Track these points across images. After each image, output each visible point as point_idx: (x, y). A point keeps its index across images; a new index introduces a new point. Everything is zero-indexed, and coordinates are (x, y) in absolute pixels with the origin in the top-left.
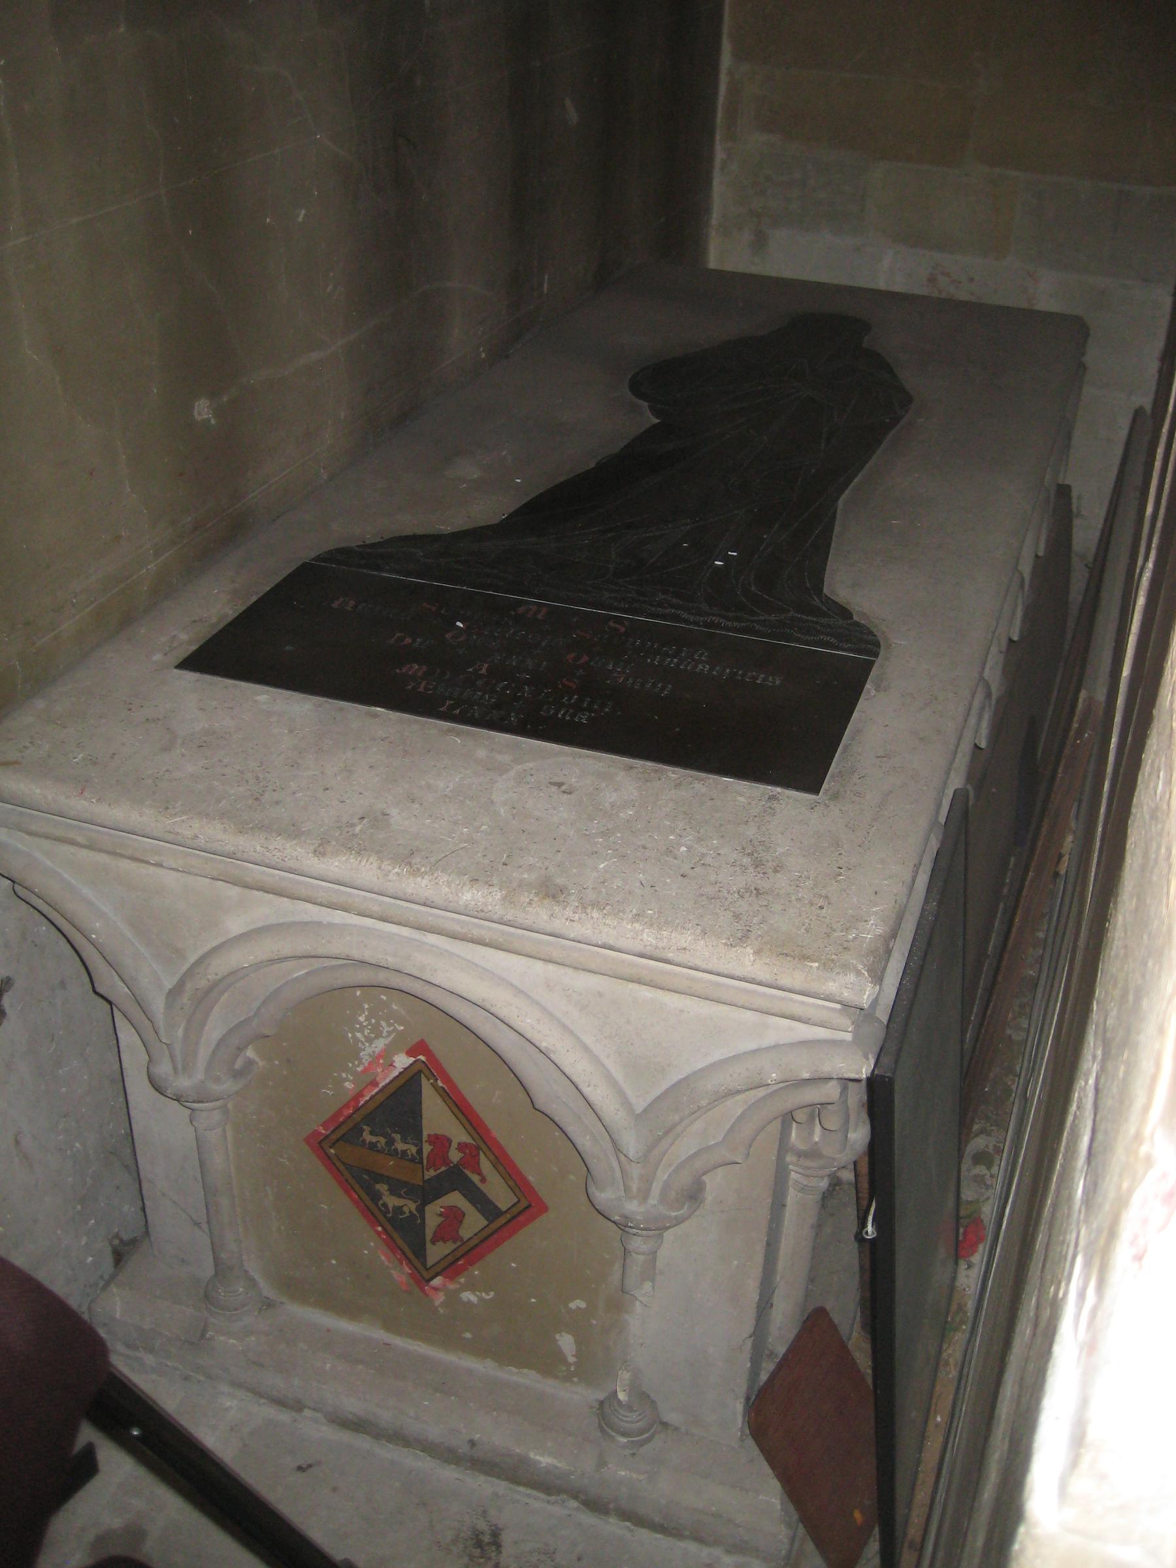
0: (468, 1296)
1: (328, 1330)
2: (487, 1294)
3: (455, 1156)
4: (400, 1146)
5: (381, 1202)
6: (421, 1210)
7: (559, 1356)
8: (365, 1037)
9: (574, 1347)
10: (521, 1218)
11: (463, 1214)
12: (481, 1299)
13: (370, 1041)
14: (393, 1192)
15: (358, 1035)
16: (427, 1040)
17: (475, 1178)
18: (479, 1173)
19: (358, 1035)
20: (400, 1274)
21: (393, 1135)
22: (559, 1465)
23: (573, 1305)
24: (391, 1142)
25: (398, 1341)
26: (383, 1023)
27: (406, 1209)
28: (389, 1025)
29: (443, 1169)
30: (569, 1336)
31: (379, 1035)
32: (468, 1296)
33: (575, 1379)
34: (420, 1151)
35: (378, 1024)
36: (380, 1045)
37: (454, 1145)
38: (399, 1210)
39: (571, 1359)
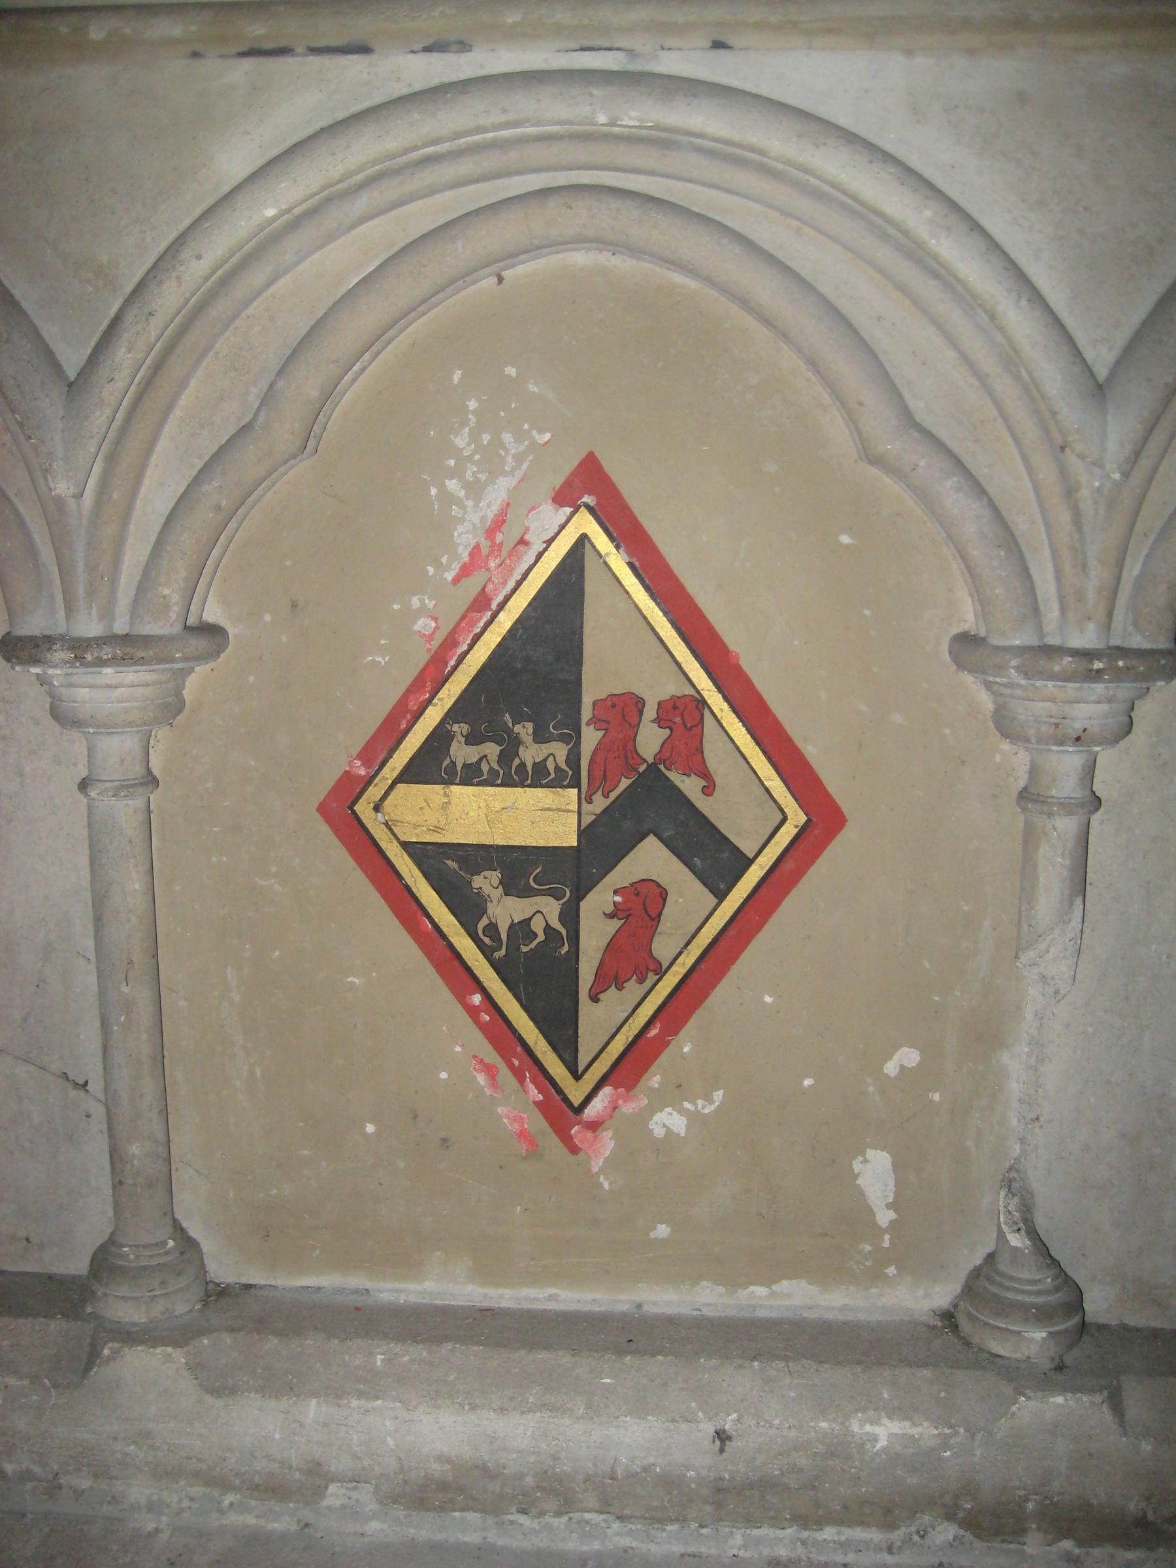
0: (669, 1121)
1: (357, 1309)
2: (709, 1099)
3: (650, 740)
4: (530, 753)
5: (484, 922)
6: (571, 917)
7: (857, 1217)
8: (467, 486)
9: (891, 1183)
10: (544, 251)
11: (663, 895)
12: (694, 1118)
13: (475, 490)
14: (513, 886)
15: (452, 485)
16: (597, 454)
17: (690, 786)
18: (705, 774)
19: (452, 485)
20: (514, 1106)
21: (518, 728)
22: (916, 1431)
23: (891, 1068)
24: (511, 747)
25: (356, 1281)
26: (507, 437)
27: (538, 926)
28: (519, 436)
29: (625, 783)
30: (885, 1154)
31: (494, 469)
32: (669, 1121)
33: (891, 1270)
34: (574, 759)
35: (498, 443)
36: (497, 495)
37: (650, 712)
38: (522, 929)
39: (885, 1217)
